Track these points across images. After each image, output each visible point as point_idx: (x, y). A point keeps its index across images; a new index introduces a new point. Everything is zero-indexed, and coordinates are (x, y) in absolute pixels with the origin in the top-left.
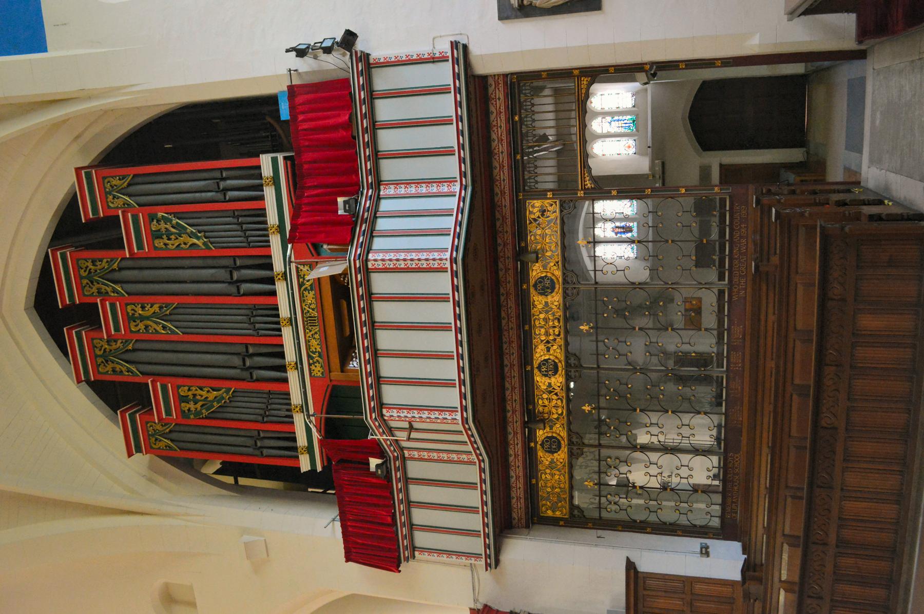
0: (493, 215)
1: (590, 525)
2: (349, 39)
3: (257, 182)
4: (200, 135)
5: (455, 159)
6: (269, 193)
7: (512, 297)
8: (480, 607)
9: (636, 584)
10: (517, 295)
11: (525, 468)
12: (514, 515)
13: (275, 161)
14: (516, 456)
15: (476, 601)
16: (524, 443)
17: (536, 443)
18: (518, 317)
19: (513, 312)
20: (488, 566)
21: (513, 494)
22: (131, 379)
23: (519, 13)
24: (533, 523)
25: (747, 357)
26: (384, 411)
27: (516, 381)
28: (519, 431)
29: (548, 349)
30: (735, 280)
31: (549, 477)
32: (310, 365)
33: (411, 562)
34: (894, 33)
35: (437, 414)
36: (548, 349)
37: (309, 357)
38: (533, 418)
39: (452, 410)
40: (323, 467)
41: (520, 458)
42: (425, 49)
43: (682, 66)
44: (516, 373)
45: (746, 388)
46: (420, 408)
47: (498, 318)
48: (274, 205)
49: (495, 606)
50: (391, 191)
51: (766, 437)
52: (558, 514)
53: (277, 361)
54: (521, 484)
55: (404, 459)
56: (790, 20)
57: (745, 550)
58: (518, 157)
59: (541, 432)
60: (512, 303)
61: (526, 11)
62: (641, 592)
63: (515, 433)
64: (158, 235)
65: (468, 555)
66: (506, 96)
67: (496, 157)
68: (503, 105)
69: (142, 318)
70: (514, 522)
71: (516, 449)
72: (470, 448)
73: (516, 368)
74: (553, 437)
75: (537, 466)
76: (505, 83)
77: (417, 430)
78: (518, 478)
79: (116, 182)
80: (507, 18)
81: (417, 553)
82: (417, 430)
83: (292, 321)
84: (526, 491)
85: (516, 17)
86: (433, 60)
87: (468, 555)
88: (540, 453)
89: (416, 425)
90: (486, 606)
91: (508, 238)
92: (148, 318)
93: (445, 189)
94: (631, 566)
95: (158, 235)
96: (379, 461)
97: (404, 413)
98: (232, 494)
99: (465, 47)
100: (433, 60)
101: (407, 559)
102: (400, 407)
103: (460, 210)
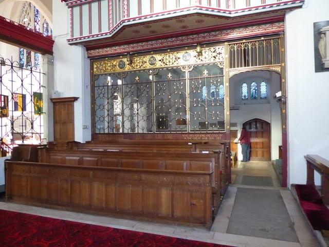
8: (53, 39)
9: (69, 101)
11: (111, 54)
17: (122, 58)
18: (173, 46)
19: (175, 43)
20: (69, 40)
24: (90, 59)
25: (160, 141)
27: (146, 47)
28: (126, 50)
29: (160, 61)
30: (191, 136)
31: (109, 65)
33: (67, 7)
34: (302, 204)
35: (126, 8)
36: (160, 61)
38: (132, 55)
39: (128, 15)
41: (115, 52)
43: (284, 127)
44: (149, 47)
45: (148, 141)
47: (171, 36)
49: (54, 45)
51: (126, 150)
52: (95, 70)
56: (305, 157)
57: (88, 142)
61: (319, 34)
62: (66, 103)
65: (72, 32)
67: (244, 30)
68: (270, 31)
70: (89, 51)
73: (151, 47)
74: (125, 65)
76: (279, 31)
80: (314, 27)
84: (102, 55)
87: (72, 32)
88: (118, 60)
91: (208, 38)
94: (76, 99)
98: (297, 198)
101: (67, 4)
103: (219, 11)
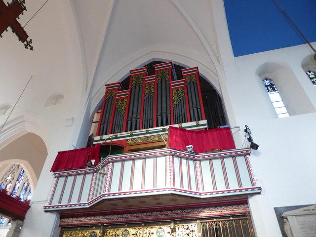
0: (189, 208)
1: (178, 222)
2: (254, 146)
3: (197, 119)
4: (211, 104)
5: (212, 190)
6: (194, 123)
7: (156, 218)
8: (30, 204)
10: (156, 219)
11: (85, 224)
12: (66, 220)
13: (205, 125)
14: (90, 220)
15: (33, 203)
16: (95, 224)
17: (95, 229)
20: (45, 207)
21: (74, 219)
22: (130, 85)
23: (279, 217)
26: (111, 163)
27: (121, 220)
32: (132, 139)
37: (135, 139)
39: (109, 190)
40: (95, 145)
42: (255, 176)
46: (111, 177)
48: (188, 125)
49: (29, 211)
50: (198, 165)
53: (134, 127)
54: (78, 222)
55: (93, 173)
58: (231, 218)
59: (99, 232)
60: (153, 217)
63: (99, 220)
64: (177, 90)
65: (52, 200)
66: (240, 213)
69: (150, 87)
70: (63, 220)
71: (93, 220)
72: (94, 198)
73: (126, 220)
75: (165, 222)
76: (246, 213)
77: (103, 177)
78: (81, 221)
79: (194, 78)
81: (57, 178)
82: (103, 177)
83: (147, 132)
84: (74, 225)
85: (277, 216)
86: (252, 180)
87: (52, 200)
89: (105, 176)
90: (30, 207)
91: (181, 215)
92: (150, 89)
93: (200, 186)
95: (177, 90)
96: (93, 163)
97: (110, 171)
99: (259, 193)
100: (252, 180)
102: (112, 169)
103: (191, 192)
